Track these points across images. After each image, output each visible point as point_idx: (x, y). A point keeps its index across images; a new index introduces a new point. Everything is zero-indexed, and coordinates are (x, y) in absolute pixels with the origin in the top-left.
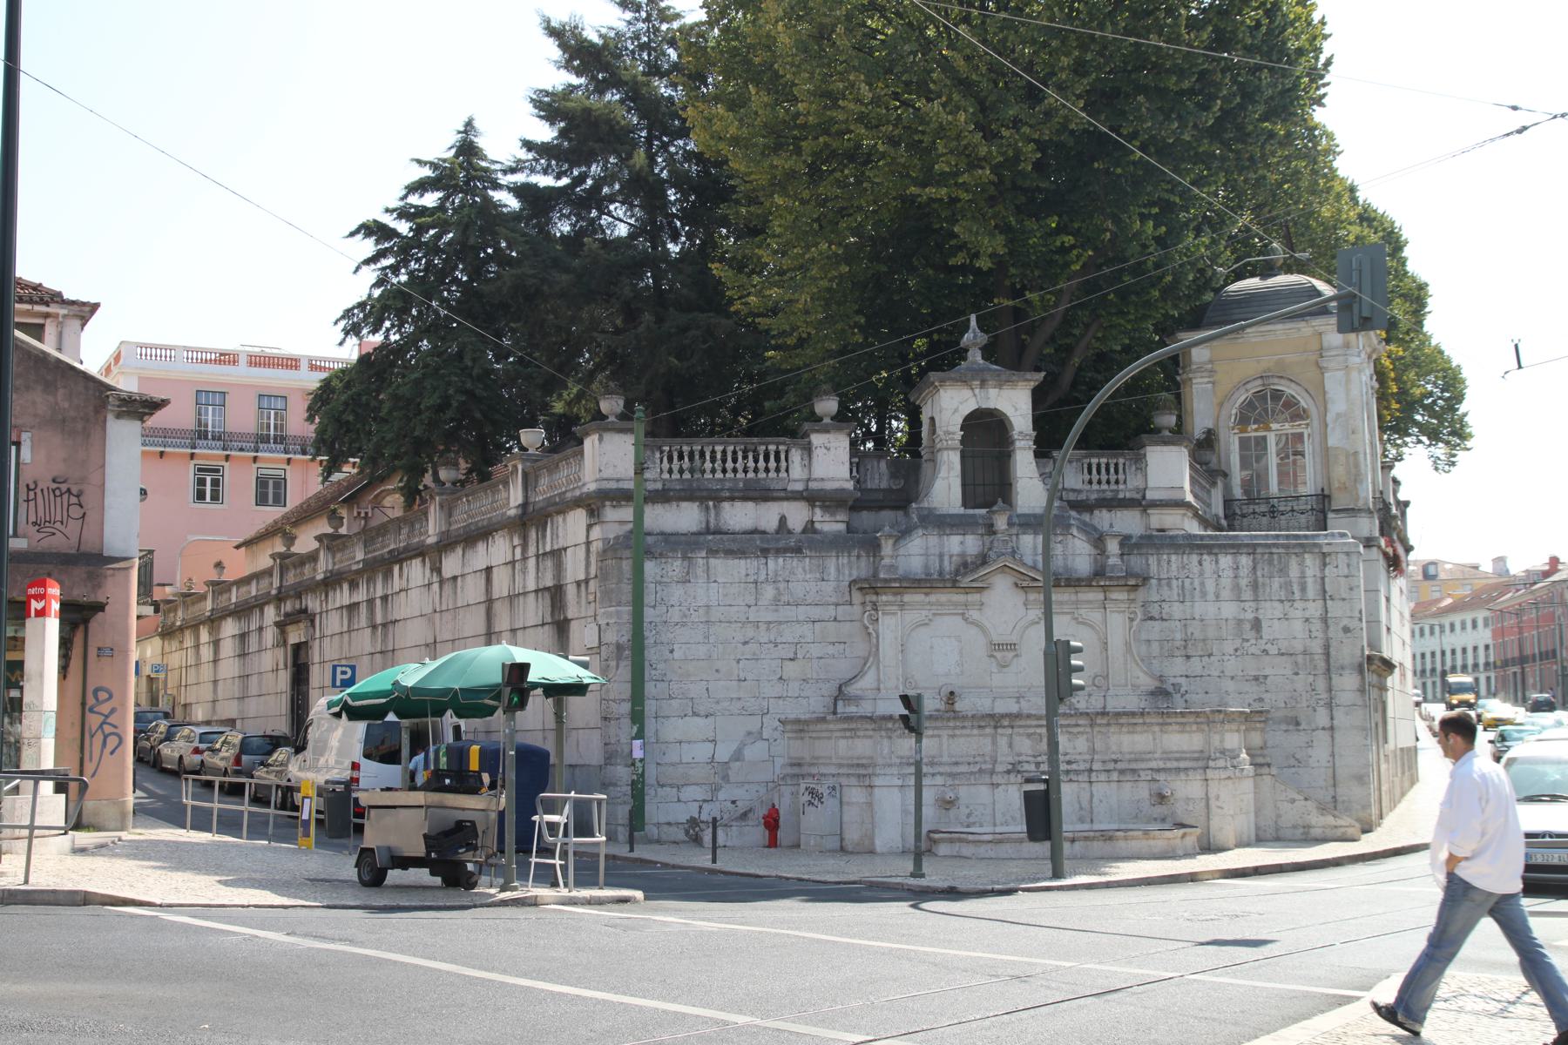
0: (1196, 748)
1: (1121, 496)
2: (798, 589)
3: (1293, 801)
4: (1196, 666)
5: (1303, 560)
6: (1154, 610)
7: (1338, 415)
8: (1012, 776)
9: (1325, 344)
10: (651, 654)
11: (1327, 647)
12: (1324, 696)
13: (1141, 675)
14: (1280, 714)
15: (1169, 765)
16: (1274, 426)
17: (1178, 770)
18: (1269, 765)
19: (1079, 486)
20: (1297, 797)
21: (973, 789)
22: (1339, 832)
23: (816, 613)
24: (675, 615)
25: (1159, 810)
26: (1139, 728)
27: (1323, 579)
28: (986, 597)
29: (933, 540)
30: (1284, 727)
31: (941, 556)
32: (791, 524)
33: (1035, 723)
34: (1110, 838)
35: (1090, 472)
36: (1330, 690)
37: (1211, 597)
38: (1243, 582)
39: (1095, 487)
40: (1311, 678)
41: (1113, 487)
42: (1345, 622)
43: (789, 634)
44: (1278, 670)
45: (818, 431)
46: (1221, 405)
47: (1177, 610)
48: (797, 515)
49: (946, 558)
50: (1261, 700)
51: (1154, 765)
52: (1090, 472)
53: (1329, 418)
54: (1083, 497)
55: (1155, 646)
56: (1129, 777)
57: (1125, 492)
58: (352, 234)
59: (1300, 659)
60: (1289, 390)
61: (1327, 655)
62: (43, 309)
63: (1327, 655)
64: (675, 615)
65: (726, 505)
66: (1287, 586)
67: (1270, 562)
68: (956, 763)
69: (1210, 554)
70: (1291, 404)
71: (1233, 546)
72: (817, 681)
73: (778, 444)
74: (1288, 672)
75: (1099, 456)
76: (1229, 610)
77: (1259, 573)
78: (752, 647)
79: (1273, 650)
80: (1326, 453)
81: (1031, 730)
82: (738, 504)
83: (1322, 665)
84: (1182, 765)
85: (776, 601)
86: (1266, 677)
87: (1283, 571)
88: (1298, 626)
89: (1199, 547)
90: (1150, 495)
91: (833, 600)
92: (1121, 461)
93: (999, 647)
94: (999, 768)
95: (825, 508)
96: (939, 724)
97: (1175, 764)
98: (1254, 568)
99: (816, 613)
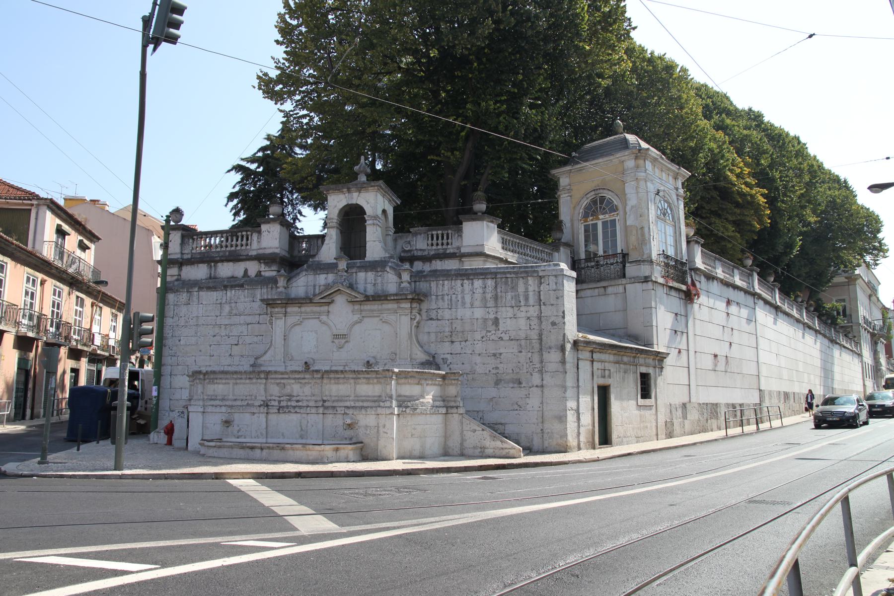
0: (377, 394)
1: (448, 252)
2: (241, 306)
3: (475, 431)
4: (457, 347)
5: (527, 282)
6: (433, 314)
7: (632, 207)
8: (262, 408)
9: (626, 167)
10: (169, 342)
11: (540, 335)
12: (538, 365)
13: (419, 353)
14: (508, 377)
15: (357, 404)
16: (601, 217)
17: (362, 407)
18: (457, 407)
19: (425, 247)
20: (478, 428)
21: (242, 415)
22: (504, 452)
23: (249, 319)
24: (182, 322)
25: (349, 433)
26: (341, 381)
27: (539, 292)
28: (332, 308)
29: (311, 277)
30: (511, 385)
31: (315, 286)
32: (250, 273)
33: (280, 376)
34: (283, 449)
35: (432, 239)
36: (542, 362)
37: (468, 305)
38: (489, 296)
39: (434, 247)
40: (530, 355)
41: (444, 247)
42: (553, 319)
43: (236, 331)
44: (508, 350)
45: (264, 223)
46: (574, 208)
47: (447, 314)
48: (253, 268)
49: (317, 287)
50: (497, 368)
51: (348, 404)
52: (432, 239)
53: (628, 208)
54: (426, 253)
55: (433, 336)
56: (330, 411)
57: (450, 250)
58: (229, 171)
59: (523, 342)
60: (608, 195)
61: (541, 339)
62: (29, 202)
63: (541, 339)
64: (182, 322)
65: (219, 264)
66: (516, 297)
67: (506, 283)
68: (235, 400)
69: (468, 279)
70: (610, 202)
71: (482, 274)
72: (248, 356)
73: (247, 231)
74: (516, 351)
75: (437, 230)
76: (479, 313)
77: (499, 290)
78: (218, 338)
79: (506, 337)
80: (626, 228)
81: (278, 381)
82: (225, 264)
83: (537, 346)
84: (365, 404)
85: (230, 314)
86: (501, 354)
87: (514, 288)
88: (522, 323)
89: (461, 275)
90: (463, 250)
91: (258, 312)
92: (450, 232)
93: (336, 336)
94: (257, 403)
95: (266, 264)
96: (228, 376)
97: (361, 404)
98: (496, 287)
99: (249, 319)
